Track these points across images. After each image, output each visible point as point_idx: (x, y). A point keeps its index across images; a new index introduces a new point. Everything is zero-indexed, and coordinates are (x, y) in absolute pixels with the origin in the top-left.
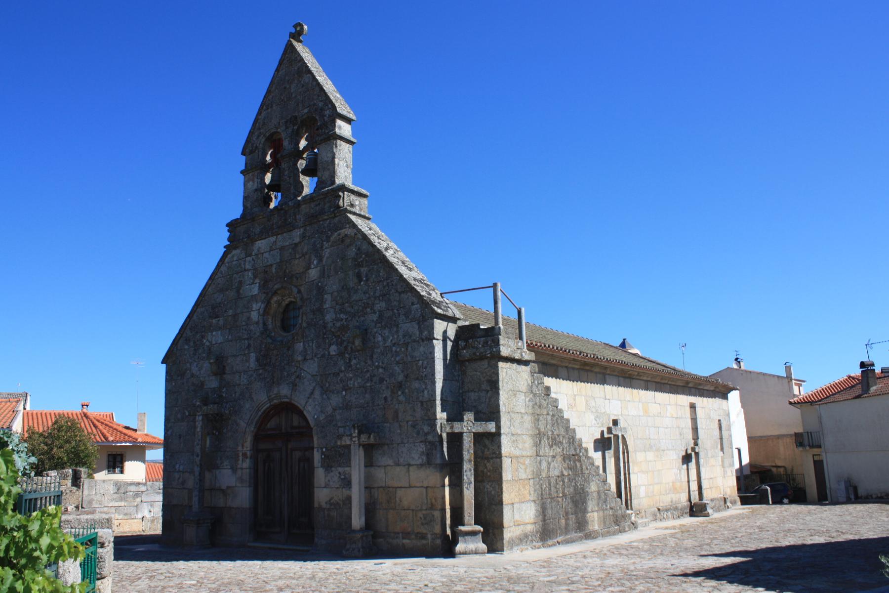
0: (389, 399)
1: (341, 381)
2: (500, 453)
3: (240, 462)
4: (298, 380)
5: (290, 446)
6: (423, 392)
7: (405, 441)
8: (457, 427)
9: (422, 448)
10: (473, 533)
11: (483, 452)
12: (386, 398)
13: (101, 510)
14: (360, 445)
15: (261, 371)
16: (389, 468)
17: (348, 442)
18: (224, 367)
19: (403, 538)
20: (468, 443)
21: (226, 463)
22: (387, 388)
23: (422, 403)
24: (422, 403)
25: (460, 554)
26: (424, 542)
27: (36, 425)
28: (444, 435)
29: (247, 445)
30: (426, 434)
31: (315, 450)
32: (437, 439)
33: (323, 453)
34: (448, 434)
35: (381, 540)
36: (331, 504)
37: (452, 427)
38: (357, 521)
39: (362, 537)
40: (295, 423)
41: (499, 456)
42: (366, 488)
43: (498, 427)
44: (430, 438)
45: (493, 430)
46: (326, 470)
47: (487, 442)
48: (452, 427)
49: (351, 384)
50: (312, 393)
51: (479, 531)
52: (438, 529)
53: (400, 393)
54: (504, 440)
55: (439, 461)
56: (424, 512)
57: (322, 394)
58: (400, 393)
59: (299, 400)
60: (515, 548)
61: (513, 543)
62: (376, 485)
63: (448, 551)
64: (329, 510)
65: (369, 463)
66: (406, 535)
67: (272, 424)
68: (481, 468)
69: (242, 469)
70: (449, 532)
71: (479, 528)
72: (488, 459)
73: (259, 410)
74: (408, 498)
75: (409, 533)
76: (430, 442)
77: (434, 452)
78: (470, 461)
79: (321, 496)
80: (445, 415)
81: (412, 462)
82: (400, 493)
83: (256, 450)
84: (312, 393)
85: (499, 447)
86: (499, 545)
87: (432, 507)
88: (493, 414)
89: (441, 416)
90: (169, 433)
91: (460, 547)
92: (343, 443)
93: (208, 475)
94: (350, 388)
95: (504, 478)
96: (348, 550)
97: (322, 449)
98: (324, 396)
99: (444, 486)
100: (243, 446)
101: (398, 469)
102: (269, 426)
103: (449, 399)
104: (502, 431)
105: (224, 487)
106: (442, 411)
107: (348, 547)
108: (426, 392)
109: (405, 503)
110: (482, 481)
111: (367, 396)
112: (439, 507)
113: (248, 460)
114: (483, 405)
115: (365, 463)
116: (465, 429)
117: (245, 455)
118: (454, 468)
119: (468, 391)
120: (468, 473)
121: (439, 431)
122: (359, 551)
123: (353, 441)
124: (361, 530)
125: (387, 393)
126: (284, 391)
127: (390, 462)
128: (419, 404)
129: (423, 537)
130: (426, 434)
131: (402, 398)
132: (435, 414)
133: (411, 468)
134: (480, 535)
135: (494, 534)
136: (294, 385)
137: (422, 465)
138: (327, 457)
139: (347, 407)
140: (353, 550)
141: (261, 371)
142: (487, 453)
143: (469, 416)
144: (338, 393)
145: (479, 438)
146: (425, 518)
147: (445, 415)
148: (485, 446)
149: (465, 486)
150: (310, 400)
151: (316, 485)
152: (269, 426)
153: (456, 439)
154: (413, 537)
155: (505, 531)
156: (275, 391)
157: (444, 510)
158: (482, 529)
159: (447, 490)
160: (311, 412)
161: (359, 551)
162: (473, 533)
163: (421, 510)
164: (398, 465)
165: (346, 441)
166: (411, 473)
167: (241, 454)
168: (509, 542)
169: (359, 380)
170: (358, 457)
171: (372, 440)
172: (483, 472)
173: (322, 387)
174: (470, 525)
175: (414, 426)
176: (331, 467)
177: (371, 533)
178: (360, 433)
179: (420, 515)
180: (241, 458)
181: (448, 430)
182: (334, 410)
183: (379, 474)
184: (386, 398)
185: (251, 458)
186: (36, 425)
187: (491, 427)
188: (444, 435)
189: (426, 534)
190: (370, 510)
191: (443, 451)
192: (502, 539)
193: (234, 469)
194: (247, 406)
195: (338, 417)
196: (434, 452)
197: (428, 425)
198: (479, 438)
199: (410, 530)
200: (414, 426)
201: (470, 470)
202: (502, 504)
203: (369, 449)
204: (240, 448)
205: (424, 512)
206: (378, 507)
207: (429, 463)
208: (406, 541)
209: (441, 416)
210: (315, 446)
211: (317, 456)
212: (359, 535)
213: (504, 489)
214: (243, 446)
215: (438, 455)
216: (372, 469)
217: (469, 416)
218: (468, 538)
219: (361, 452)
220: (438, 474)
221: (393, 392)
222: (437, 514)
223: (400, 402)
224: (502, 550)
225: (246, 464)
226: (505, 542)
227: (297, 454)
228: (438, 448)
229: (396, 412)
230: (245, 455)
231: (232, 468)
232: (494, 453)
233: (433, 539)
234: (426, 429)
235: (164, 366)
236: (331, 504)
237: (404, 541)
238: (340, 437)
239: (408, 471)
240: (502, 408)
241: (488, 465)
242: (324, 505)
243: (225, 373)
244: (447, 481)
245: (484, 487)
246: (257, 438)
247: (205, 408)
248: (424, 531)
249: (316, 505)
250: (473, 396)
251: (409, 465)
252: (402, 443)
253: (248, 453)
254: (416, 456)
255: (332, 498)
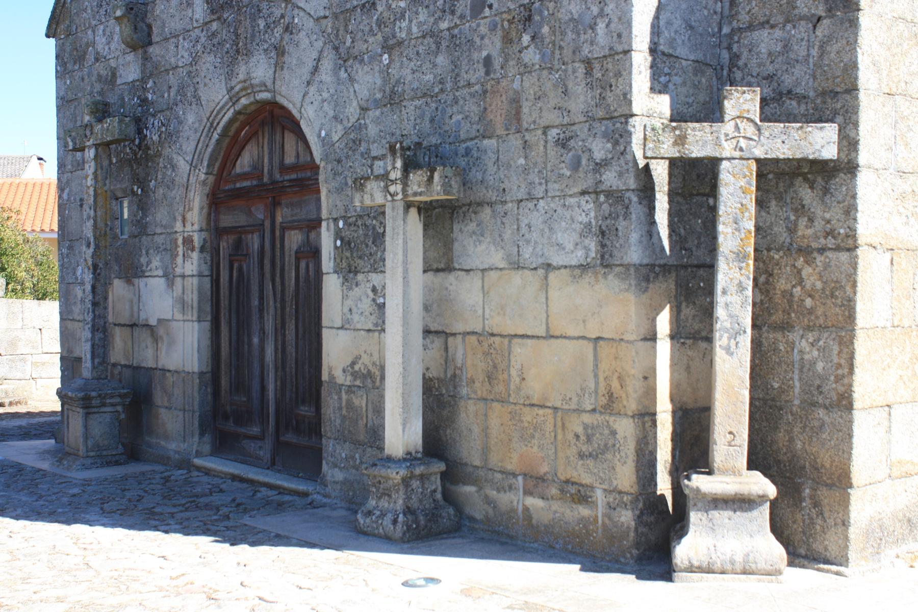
0: (497, 63)
1: (380, 23)
2: (852, 234)
3: (180, 259)
4: (287, 37)
5: (279, 219)
6: (593, 27)
7: (539, 191)
8: (700, 141)
9: (586, 211)
10: (742, 503)
11: (792, 230)
12: (488, 61)
13: (37, 358)
14: (408, 206)
15: (215, 26)
16: (493, 275)
17: (379, 199)
18: (150, 27)
19: (527, 492)
20: (736, 196)
21: (156, 263)
22: (493, 28)
23: (588, 63)
24: (588, 63)
25: (691, 569)
26: (584, 511)
27: (31, 215)
28: (660, 172)
29: (191, 219)
30: (600, 166)
31: (324, 224)
32: (632, 183)
33: (338, 235)
34: (674, 163)
35: (470, 489)
36: (355, 375)
37: (681, 140)
38: (402, 431)
39: (406, 482)
40: (290, 159)
41: (848, 244)
42: (427, 332)
43: (849, 143)
44: (610, 178)
45: (830, 152)
46: (346, 280)
47: (807, 195)
48: (681, 140)
49: (402, 30)
50: (316, 69)
51: (763, 498)
52: (625, 477)
53: (526, 39)
54: (866, 185)
55: (635, 255)
56: (587, 418)
57: (337, 69)
58: (526, 39)
59: (291, 96)
60: (889, 553)
61: (881, 537)
62: (459, 327)
63: (651, 545)
64: (350, 389)
65: (441, 261)
66: (536, 483)
67: (244, 163)
68: (782, 284)
69: (183, 276)
70: (664, 486)
71: (762, 485)
72: (806, 252)
73: (212, 128)
74: (543, 370)
75: (542, 479)
76: (609, 194)
77: (622, 224)
78: (741, 257)
79: (337, 351)
80: (663, 104)
81: (557, 259)
82: (521, 352)
83: (215, 230)
84: (316, 69)
85: (850, 211)
86: (830, 543)
87: (610, 405)
88: (833, 98)
89: (649, 106)
90: (65, 196)
91: (685, 550)
92: (368, 202)
93: (118, 288)
94: (400, 43)
95: (862, 319)
96: (369, 513)
97: (336, 220)
98: (343, 75)
99: (651, 338)
100: (184, 221)
101: (517, 278)
102: (238, 169)
103: (682, 51)
104: (863, 158)
105: (153, 322)
106: (658, 87)
107: (372, 503)
108: (601, 26)
109: (535, 387)
110: (785, 327)
111: (441, 60)
112: (632, 406)
113: (195, 255)
114: (798, 71)
115: (426, 260)
116: (727, 149)
117: (188, 241)
118: (687, 277)
119: (751, 27)
120: (734, 299)
121: (639, 154)
122: (395, 522)
123: (391, 197)
124: (409, 458)
125: (492, 46)
126: (259, 69)
127: (497, 258)
128: (581, 70)
129: (582, 497)
130: (600, 166)
131: (531, 56)
132: (626, 99)
133: (552, 276)
134: (768, 505)
135: (816, 504)
136: (280, 51)
137: (583, 268)
138: (347, 243)
139: (392, 98)
140: (383, 515)
141: (215, 26)
142: (804, 230)
143: (742, 102)
144: (372, 58)
145: (777, 180)
146: (589, 439)
147: (663, 104)
148: (801, 209)
149: (721, 340)
150: (312, 89)
151: (325, 322)
152: (238, 169)
153: (696, 181)
154: (554, 491)
155: (855, 495)
156: (242, 71)
157: (648, 416)
158: (771, 490)
159: (664, 348)
160: (315, 121)
161: (395, 522)
162: (742, 503)
163: (579, 411)
164: (517, 266)
165: (374, 195)
166: (554, 294)
167: (180, 241)
168: (867, 533)
169: (423, 16)
170: (405, 239)
171: (437, 193)
172: (788, 295)
173: (336, 49)
174: (735, 472)
175: (563, 144)
176: (356, 272)
177: (442, 466)
178: (409, 166)
179: (576, 425)
180: (180, 250)
181: (668, 148)
182: (364, 109)
183: (467, 292)
184: (488, 61)
185: (202, 249)
186: (31, 215)
187: (822, 141)
188: (660, 172)
189: (592, 488)
190: (439, 401)
191: (653, 223)
192: (845, 524)
193: (169, 277)
194: (191, 118)
195: (373, 130)
196: (622, 224)
197: (607, 136)
198: (777, 180)
199: (544, 469)
200: (563, 144)
201: (741, 288)
202: (850, 407)
203: (439, 218)
204: (178, 226)
205: (587, 418)
206: (464, 391)
207: (605, 261)
208: (533, 502)
209: (649, 106)
210: (324, 214)
211: (327, 242)
212: (396, 475)
213: (859, 359)
214: (184, 221)
215: (634, 237)
216: (451, 277)
217: (742, 102)
218: (722, 516)
219: (415, 224)
220: (631, 297)
221: (507, 40)
222: (626, 428)
223: (526, 70)
224: (843, 561)
225: (191, 265)
226: (853, 532)
227: (294, 239)
228: (637, 210)
229: (516, 102)
230: (188, 241)
231: (165, 275)
232: (830, 233)
233: (610, 507)
234: (600, 149)
235: (52, 41)
236: (355, 375)
237: (531, 501)
238: (360, 183)
239: (545, 285)
240: (866, 78)
241: (807, 271)
242: (341, 378)
243: (150, 43)
244: (664, 322)
245: (792, 345)
246: (217, 200)
247: (98, 128)
248: (586, 479)
249: (325, 377)
250: (765, 41)
251: (548, 267)
252: (531, 198)
253: (197, 239)
254: (567, 238)
255: (359, 357)
